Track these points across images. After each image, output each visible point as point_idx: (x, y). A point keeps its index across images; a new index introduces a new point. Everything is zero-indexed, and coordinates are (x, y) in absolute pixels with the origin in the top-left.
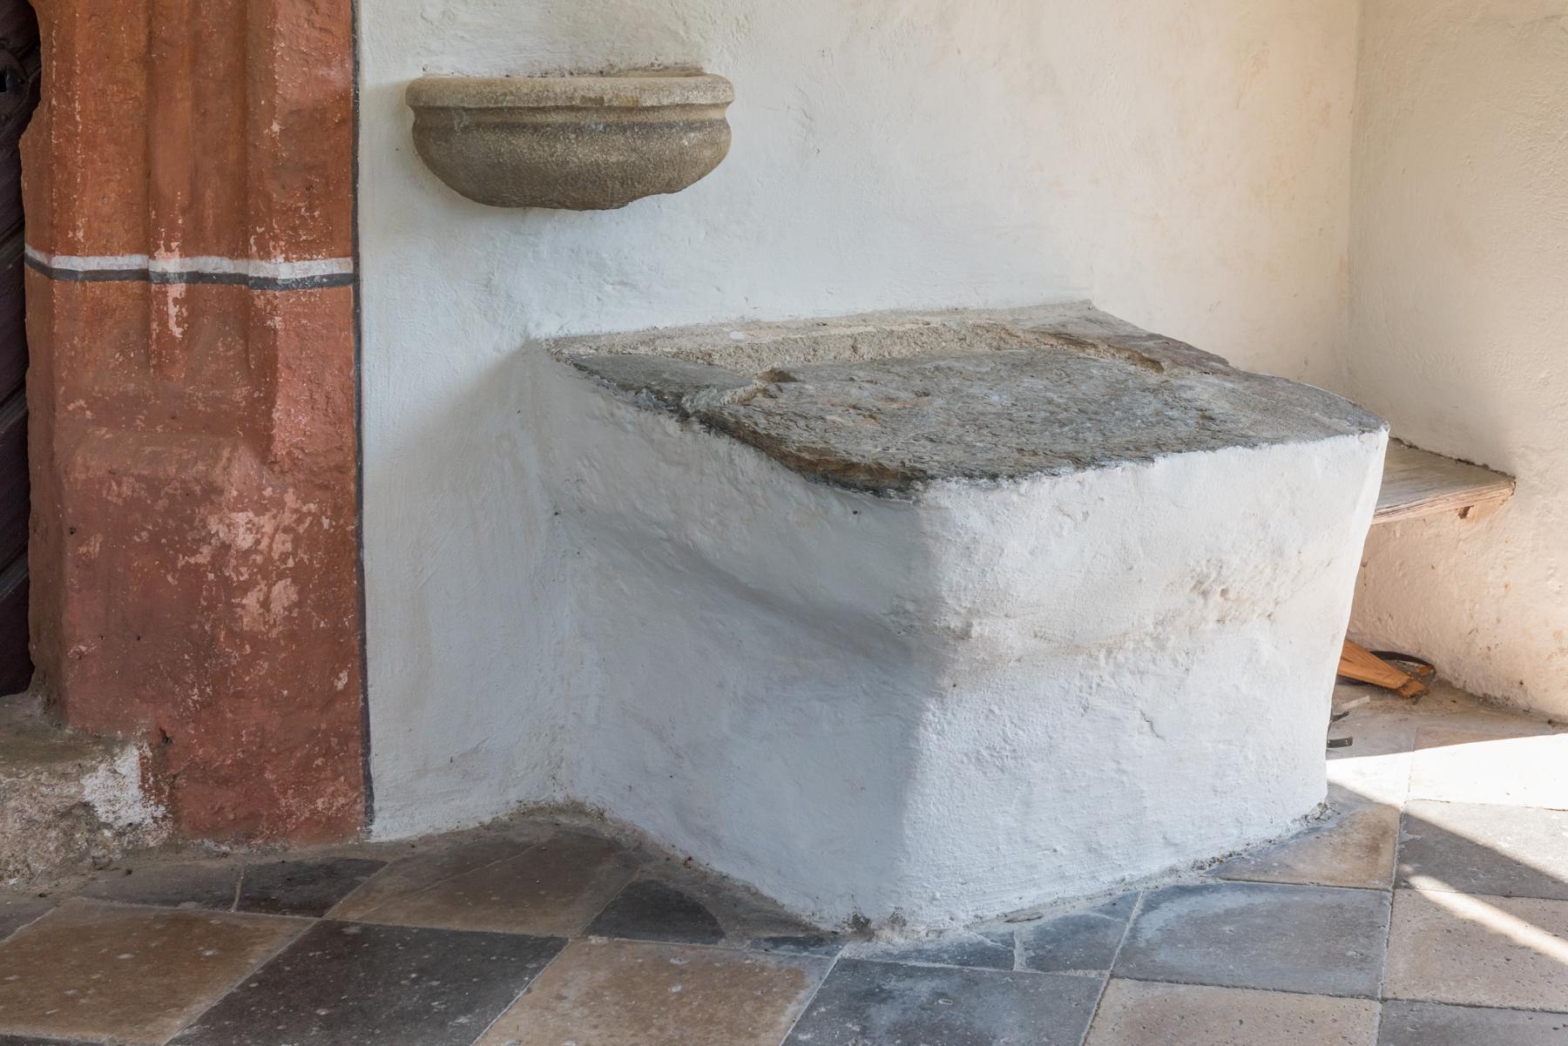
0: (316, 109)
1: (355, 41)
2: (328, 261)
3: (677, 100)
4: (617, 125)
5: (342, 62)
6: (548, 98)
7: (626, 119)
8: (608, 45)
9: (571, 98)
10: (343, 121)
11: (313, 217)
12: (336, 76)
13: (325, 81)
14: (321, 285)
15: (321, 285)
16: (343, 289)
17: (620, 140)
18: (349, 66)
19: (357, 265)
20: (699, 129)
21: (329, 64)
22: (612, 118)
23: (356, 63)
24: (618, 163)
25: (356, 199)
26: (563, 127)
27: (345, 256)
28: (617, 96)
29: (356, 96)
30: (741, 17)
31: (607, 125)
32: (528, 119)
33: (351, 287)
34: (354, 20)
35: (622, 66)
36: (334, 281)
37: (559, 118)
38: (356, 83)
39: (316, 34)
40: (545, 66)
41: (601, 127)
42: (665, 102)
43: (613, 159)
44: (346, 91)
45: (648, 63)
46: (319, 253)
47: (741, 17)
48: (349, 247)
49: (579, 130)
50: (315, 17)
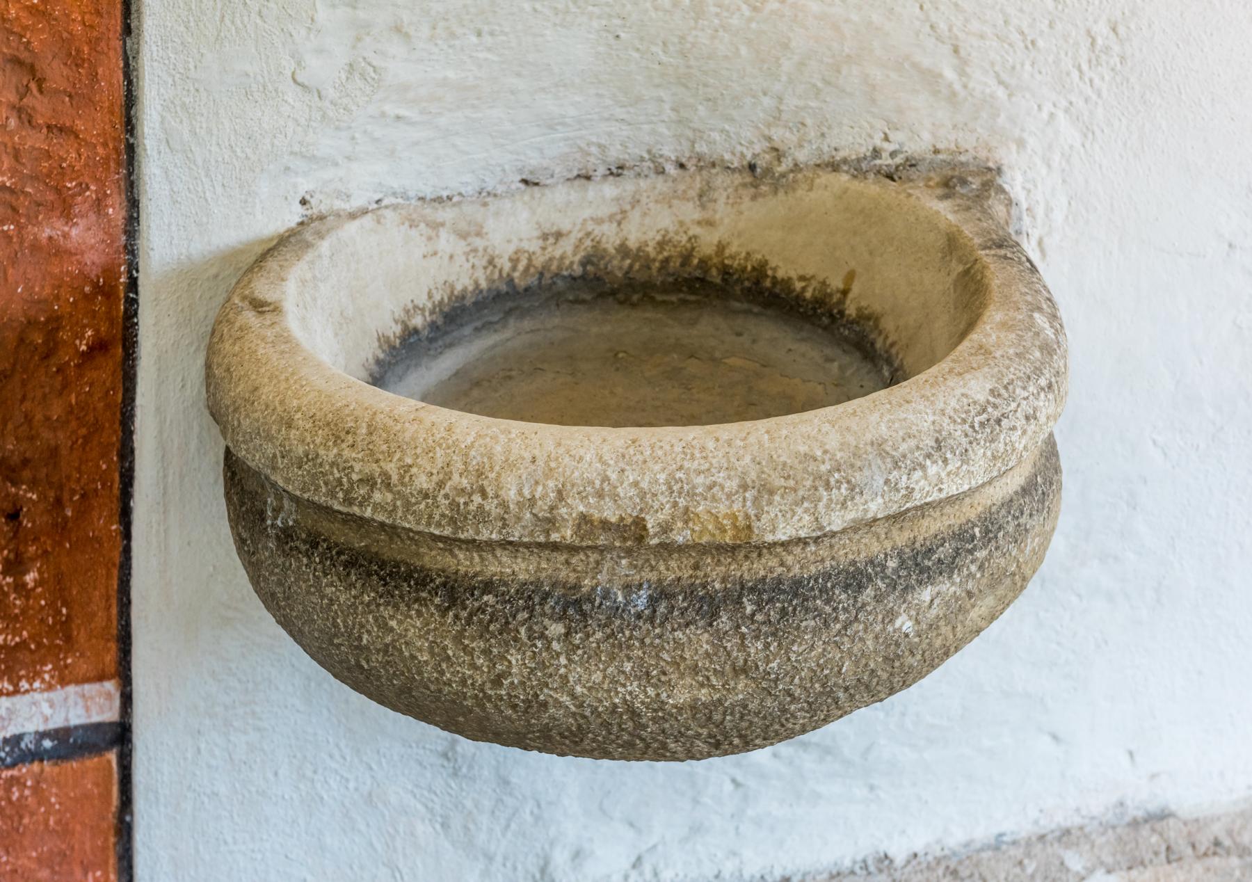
0: (31, 323)
1: (131, 149)
2: (58, 694)
3: (875, 507)
4: (690, 593)
5: (99, 205)
6: (482, 516)
7: (716, 574)
8: (767, 101)
9: (550, 522)
10: (100, 346)
11: (20, 587)
12: (85, 237)
13: (56, 251)
14: (36, 755)
15: (36, 755)
16: (92, 762)
17: (699, 641)
18: (116, 211)
19: (127, 700)
20: (949, 567)
21: (67, 214)
22: (673, 570)
23: (133, 204)
24: (694, 707)
25: (127, 535)
26: (531, 596)
27: (101, 678)
28: (687, 516)
29: (133, 284)
30: (1101, 29)
31: (662, 594)
32: (434, 559)
33: (112, 756)
34: (130, 100)
35: (802, 156)
36: (70, 744)
37: (521, 568)
38: (131, 250)
39: (36, 140)
40: (615, 154)
41: (641, 601)
42: (836, 522)
43: (681, 696)
44: (109, 271)
45: (864, 150)
46: (34, 676)
47: (1101, 29)
48: (111, 659)
49: (576, 606)
50: (35, 101)
